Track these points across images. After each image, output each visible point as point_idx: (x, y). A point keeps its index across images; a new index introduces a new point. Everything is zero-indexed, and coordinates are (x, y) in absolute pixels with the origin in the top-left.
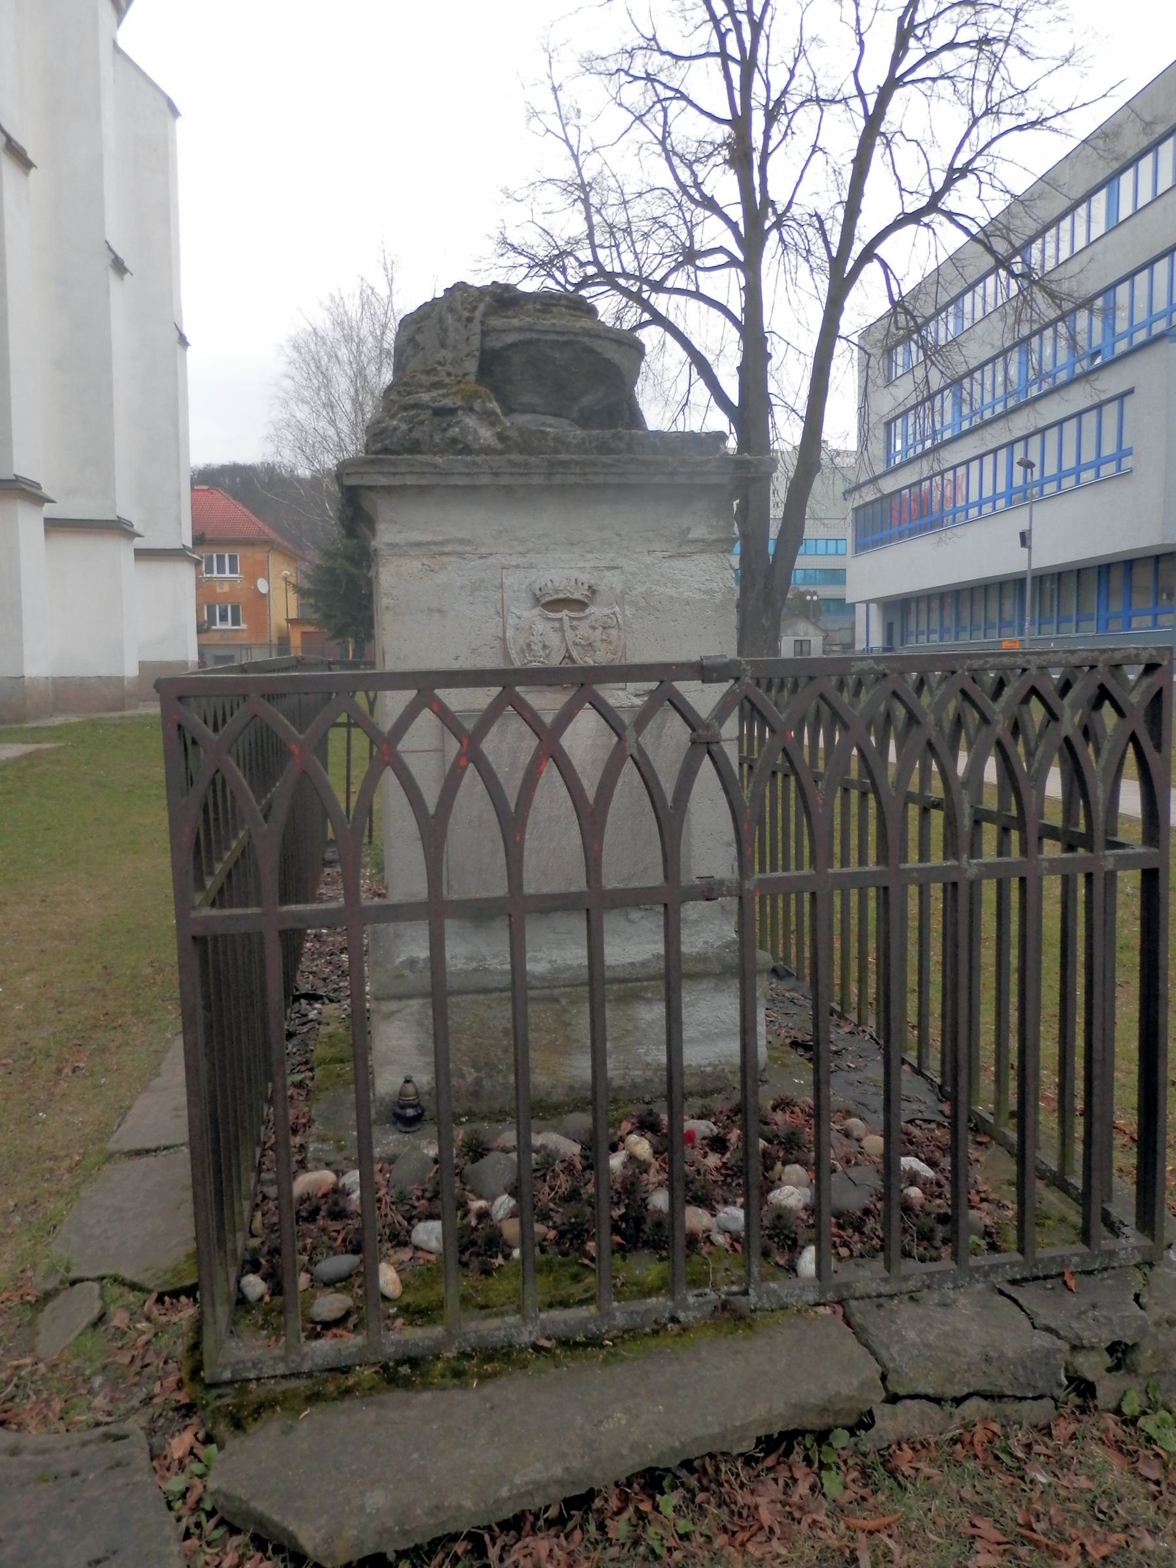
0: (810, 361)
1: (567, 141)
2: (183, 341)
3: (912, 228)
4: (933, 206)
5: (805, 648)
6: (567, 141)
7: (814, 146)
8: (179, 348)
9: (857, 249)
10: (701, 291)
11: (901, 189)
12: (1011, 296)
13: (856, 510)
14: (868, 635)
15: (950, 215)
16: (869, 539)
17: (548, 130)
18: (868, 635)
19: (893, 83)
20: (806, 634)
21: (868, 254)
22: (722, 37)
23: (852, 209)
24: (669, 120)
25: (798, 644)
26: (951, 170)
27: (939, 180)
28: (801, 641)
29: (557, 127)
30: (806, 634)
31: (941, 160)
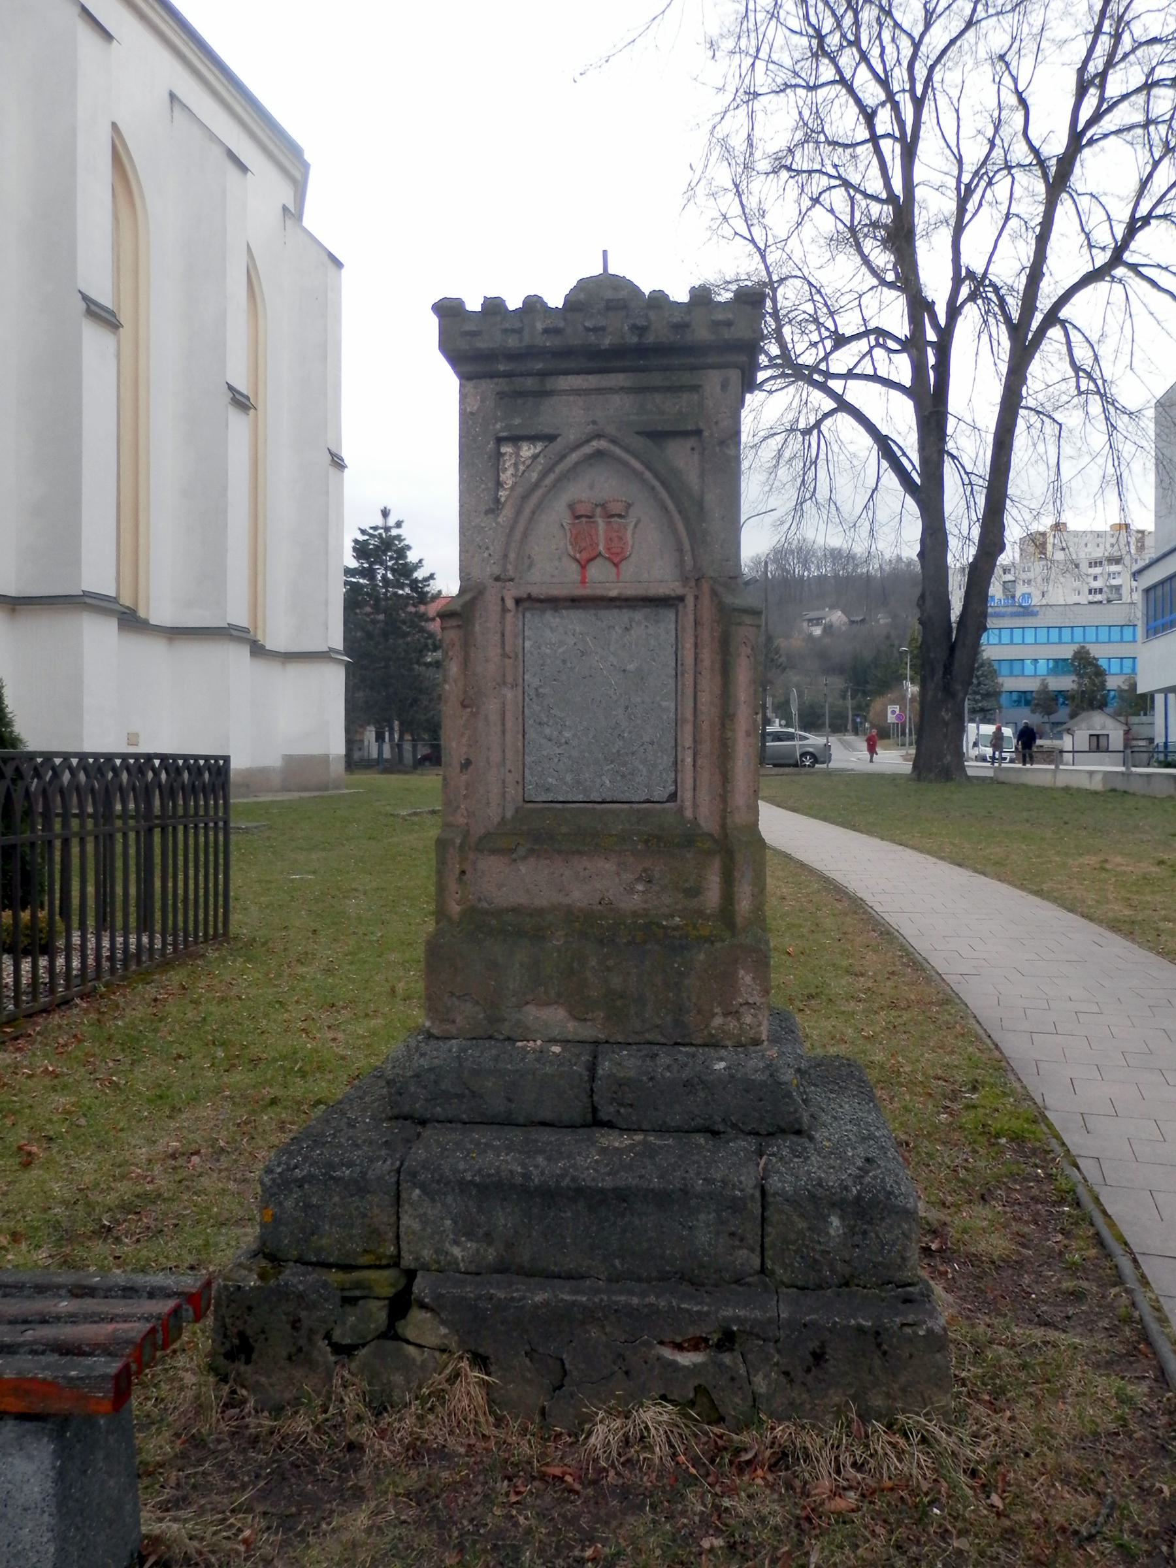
0: (990, 439)
1: (753, 241)
2: (338, 463)
3: (1102, 287)
4: (1117, 258)
5: (1103, 741)
6: (753, 241)
7: (1008, 213)
8: (332, 471)
9: (1038, 318)
10: (879, 373)
11: (1090, 246)
12: (902, 329)
13: (1147, 591)
14: (1166, 728)
15: (1134, 268)
16: (1160, 622)
17: (736, 233)
18: (1166, 728)
19: (1077, 141)
20: (1103, 728)
21: (1052, 318)
22: (869, 117)
23: (1035, 274)
24: (737, 199)
25: (1095, 739)
26: (1133, 219)
27: (1120, 231)
28: (1098, 736)
29: (744, 230)
30: (1103, 728)
31: (1122, 214)
